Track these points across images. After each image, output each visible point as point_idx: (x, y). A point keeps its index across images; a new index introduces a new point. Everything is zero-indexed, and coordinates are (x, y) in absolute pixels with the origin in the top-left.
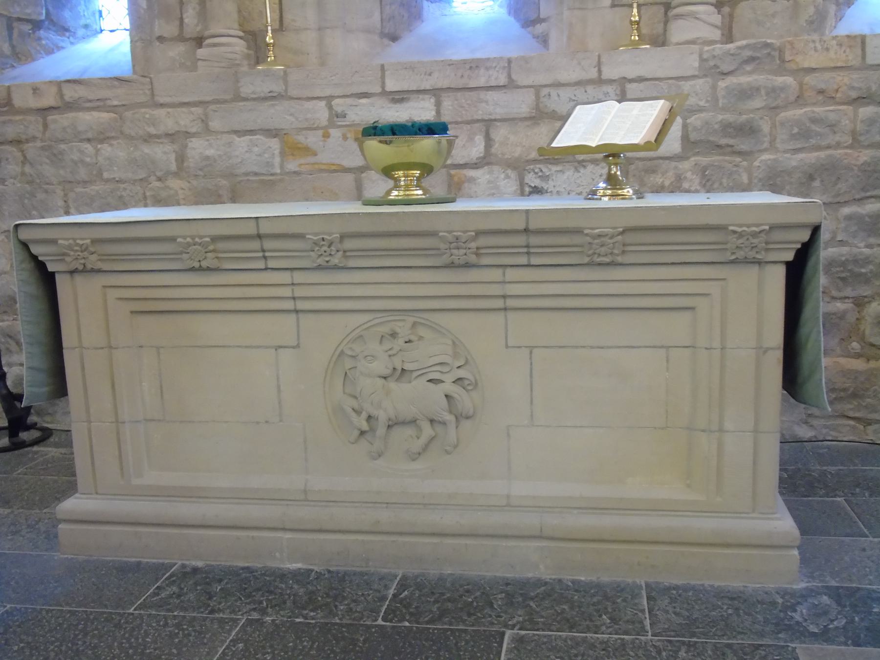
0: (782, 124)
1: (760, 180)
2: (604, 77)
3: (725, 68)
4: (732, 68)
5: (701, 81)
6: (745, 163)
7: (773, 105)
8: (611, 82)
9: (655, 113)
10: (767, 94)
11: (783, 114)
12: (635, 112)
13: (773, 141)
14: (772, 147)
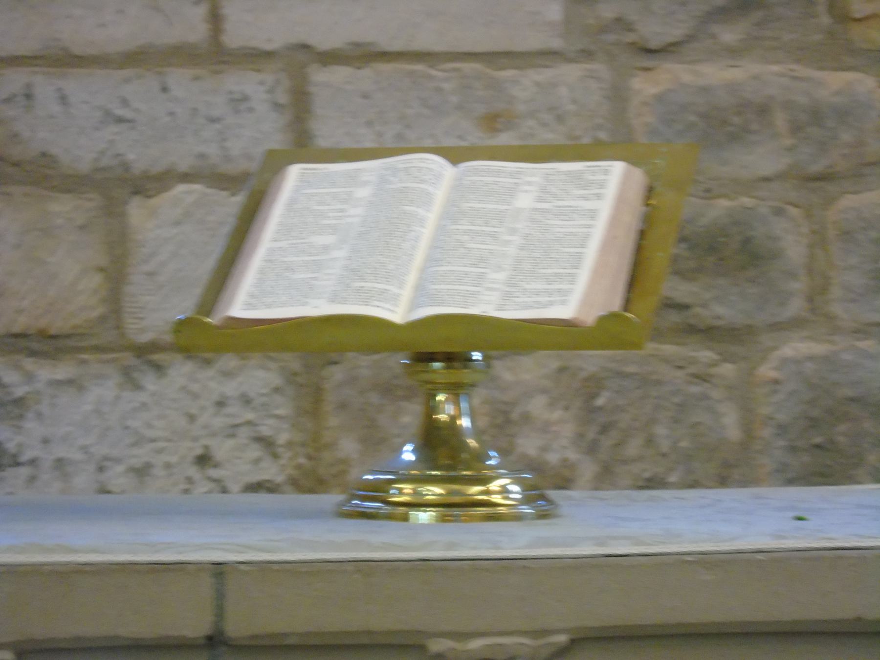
0: (846, 235)
1: (782, 429)
2: (240, 32)
3: (655, 31)
4: (676, 33)
5: (571, 72)
6: (727, 369)
7: (816, 168)
8: (255, 57)
9: (605, 208)
10: (796, 129)
11: (848, 201)
12: (525, 201)
13: (817, 294)
14: (816, 316)
